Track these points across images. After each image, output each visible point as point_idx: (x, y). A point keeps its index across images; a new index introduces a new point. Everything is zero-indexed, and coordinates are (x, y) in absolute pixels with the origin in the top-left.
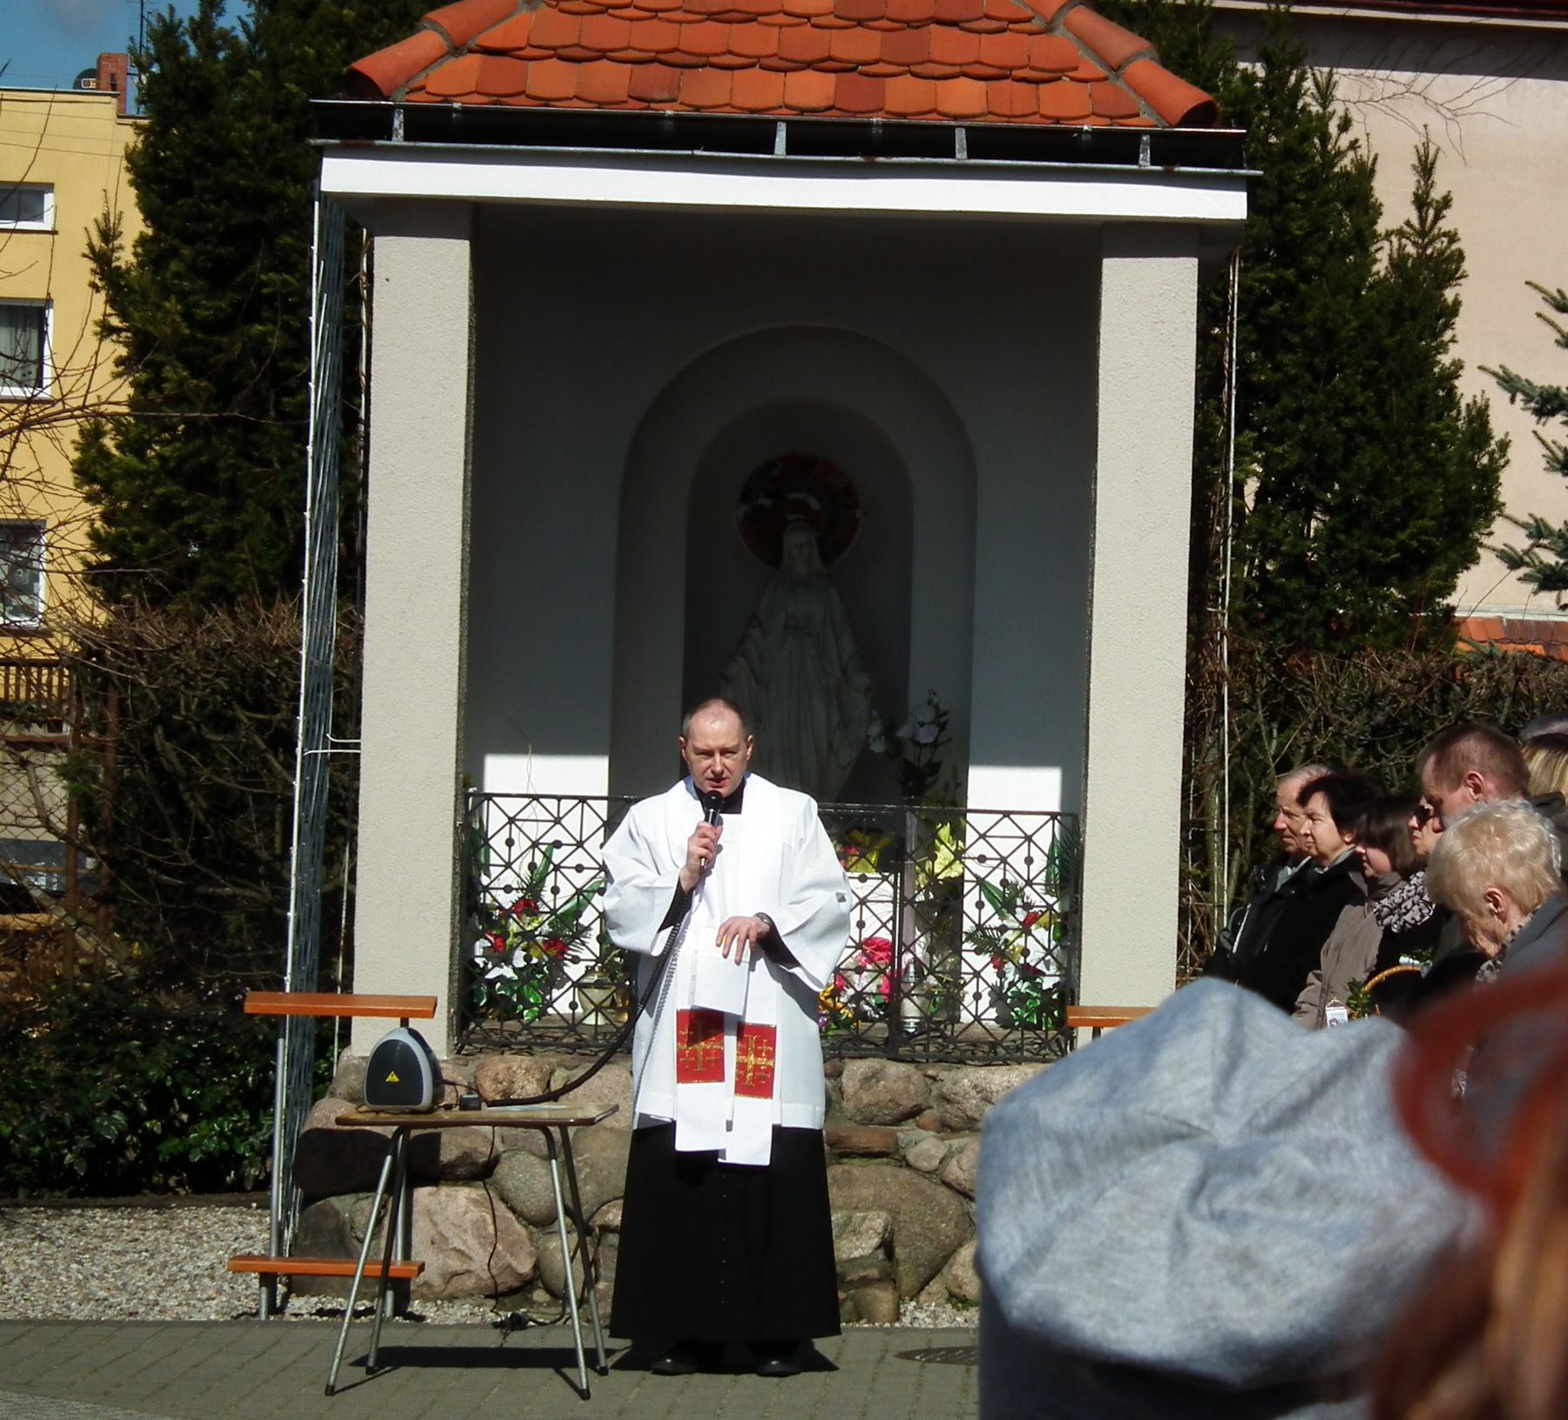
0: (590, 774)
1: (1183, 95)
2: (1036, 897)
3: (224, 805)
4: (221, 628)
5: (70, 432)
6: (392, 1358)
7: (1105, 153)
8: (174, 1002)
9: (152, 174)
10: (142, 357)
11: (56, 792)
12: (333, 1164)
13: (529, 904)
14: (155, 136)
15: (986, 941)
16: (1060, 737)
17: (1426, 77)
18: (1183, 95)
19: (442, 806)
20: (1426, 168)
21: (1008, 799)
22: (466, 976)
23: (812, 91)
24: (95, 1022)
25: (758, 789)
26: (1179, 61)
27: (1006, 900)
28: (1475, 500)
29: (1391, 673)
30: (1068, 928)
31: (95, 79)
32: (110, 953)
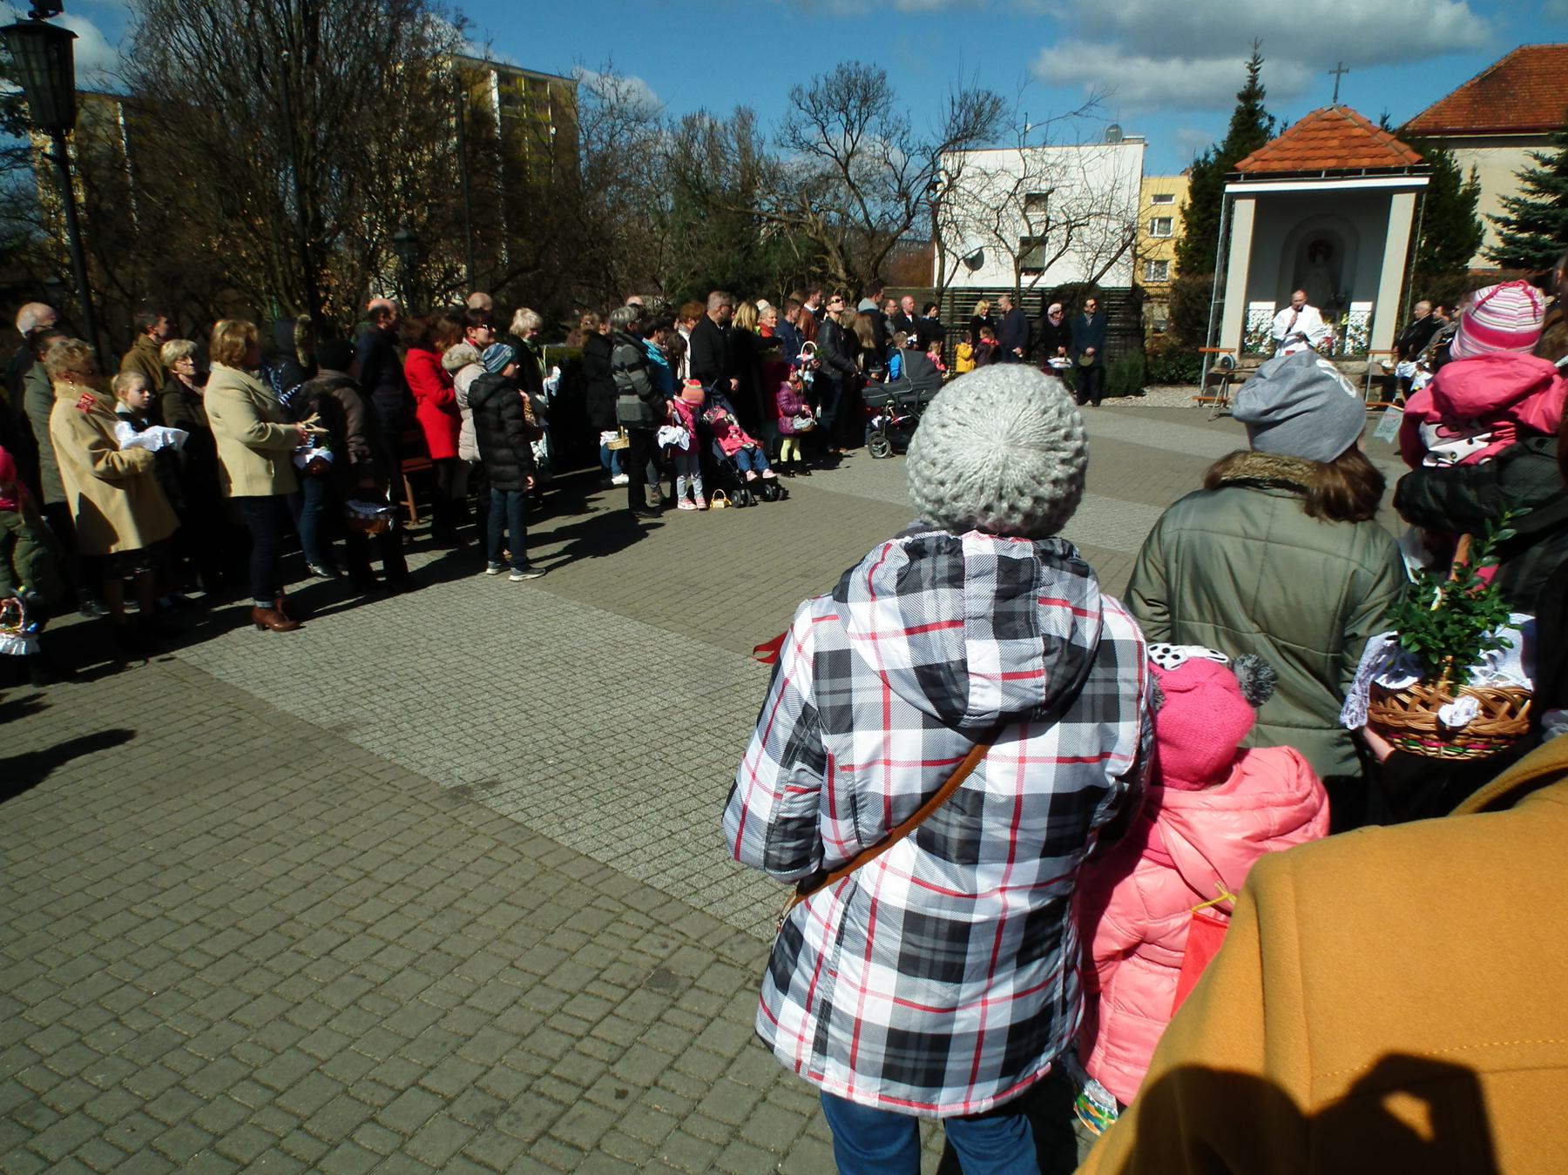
0: (1272, 305)
1: (1418, 157)
2: (1364, 328)
3: (1198, 312)
4: (1200, 279)
5: (1173, 242)
6: (1222, 415)
7: (1397, 171)
8: (1186, 350)
9: (1194, 191)
10: (1189, 227)
11: (1166, 311)
12: (1213, 380)
13: (1256, 331)
14: (1194, 183)
15: (1351, 337)
16: (1372, 295)
17: (40, 786)
18: (1418, 157)
19: (1242, 312)
20: (1474, 170)
21: (1359, 311)
22: (1243, 345)
23: (1331, 163)
24: (1171, 353)
25: (1307, 308)
26: (1417, 150)
27: (1357, 329)
28: (1477, 242)
29: (1450, 280)
30: (1370, 334)
31: (1184, 173)
32: (1174, 340)
